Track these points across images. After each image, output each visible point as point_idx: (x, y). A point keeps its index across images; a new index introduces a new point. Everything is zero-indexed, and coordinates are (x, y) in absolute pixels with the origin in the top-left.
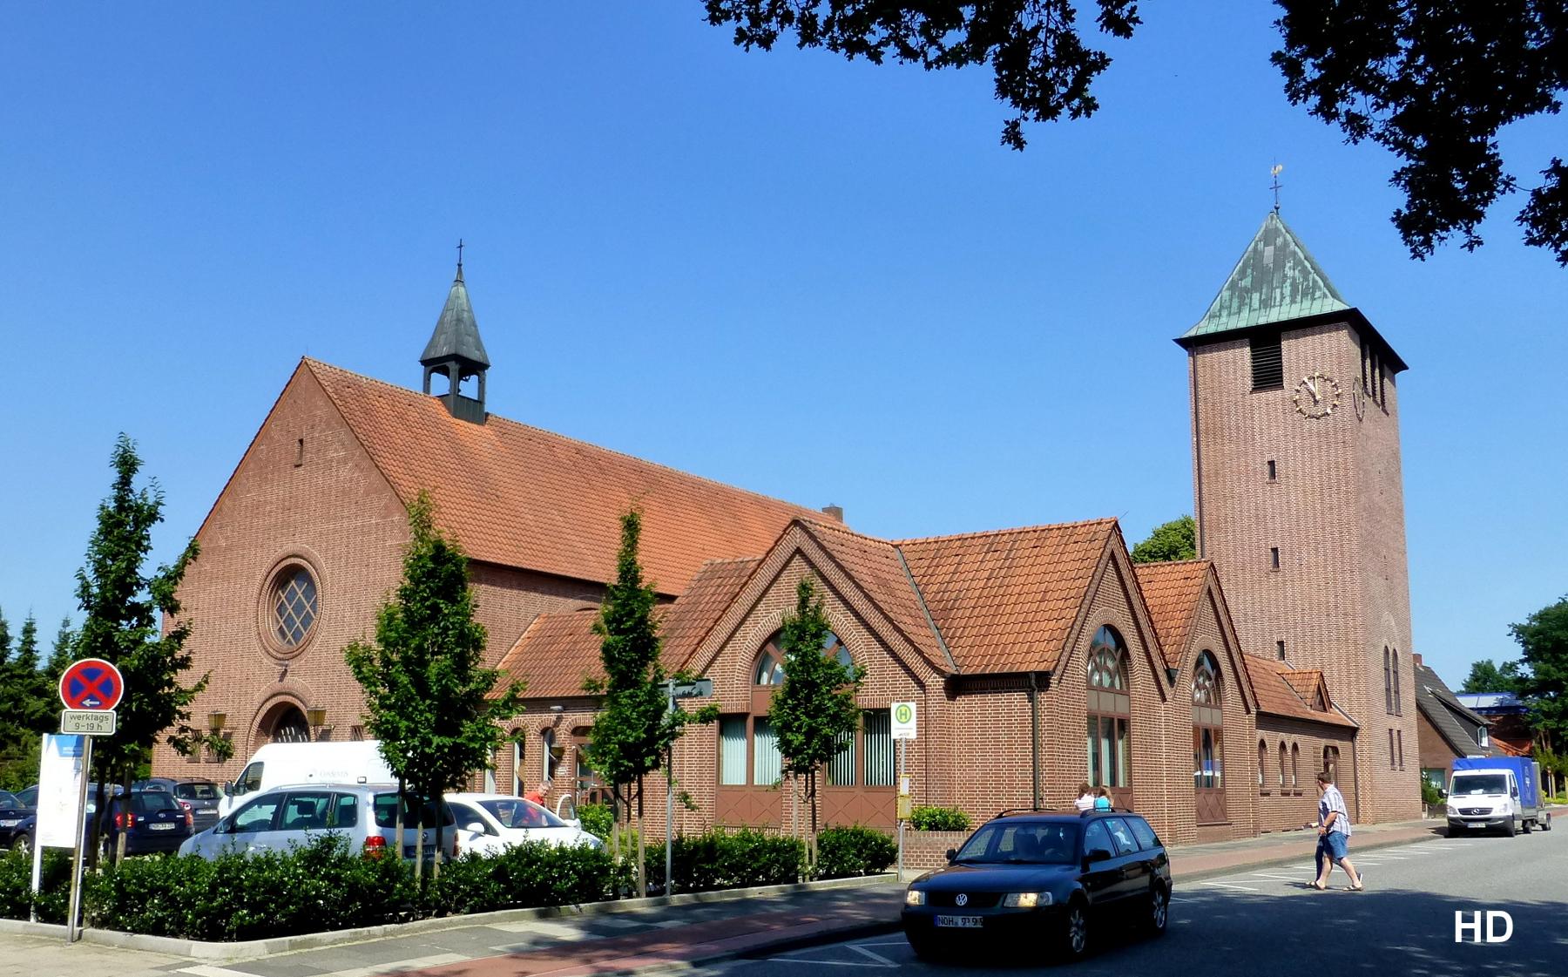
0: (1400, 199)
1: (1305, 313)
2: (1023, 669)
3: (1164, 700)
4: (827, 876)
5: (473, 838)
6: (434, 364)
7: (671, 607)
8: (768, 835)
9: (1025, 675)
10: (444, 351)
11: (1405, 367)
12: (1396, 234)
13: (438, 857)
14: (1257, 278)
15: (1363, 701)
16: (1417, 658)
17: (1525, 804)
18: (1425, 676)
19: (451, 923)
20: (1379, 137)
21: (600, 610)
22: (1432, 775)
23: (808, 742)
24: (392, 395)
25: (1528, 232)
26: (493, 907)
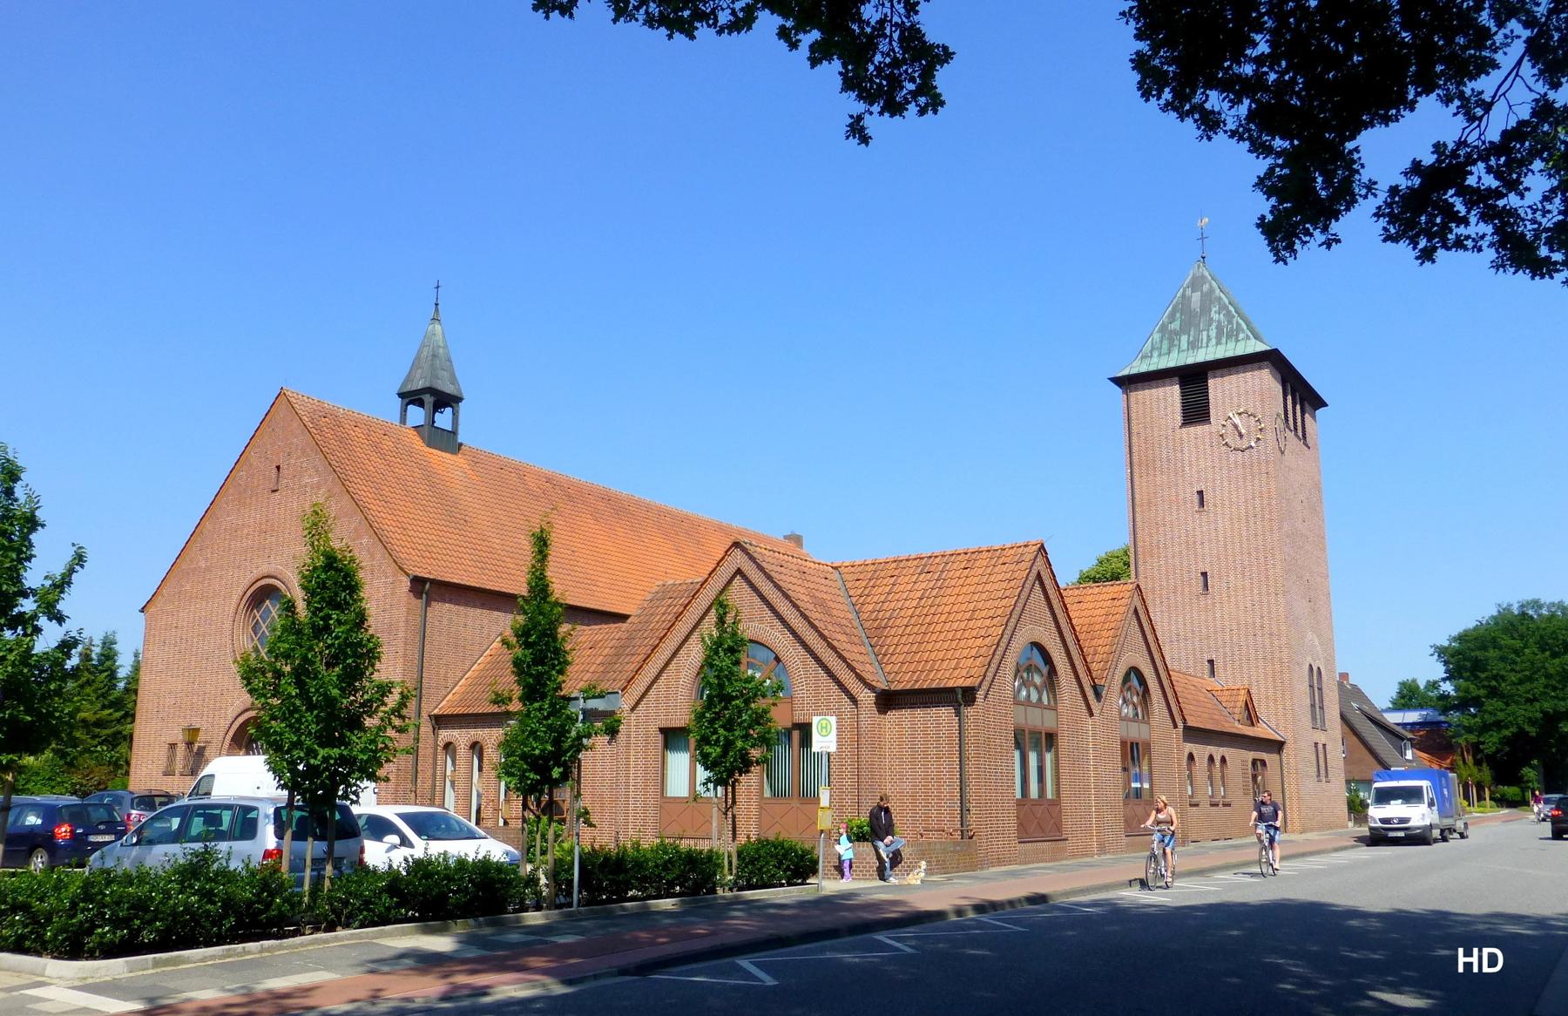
0: (1264, 206)
1: (1230, 354)
2: (950, 684)
3: (1091, 715)
4: (751, 887)
5: (388, 851)
6: (411, 397)
7: (624, 626)
8: (684, 845)
9: (952, 690)
10: (420, 384)
11: (1325, 405)
12: (1261, 241)
13: (329, 870)
14: (1188, 319)
15: (1289, 716)
16: (1344, 676)
17: (1442, 814)
18: (1350, 693)
19: (336, 939)
20: (1233, 134)
21: (505, 623)
22: (1361, 787)
23: (725, 754)
24: (368, 426)
25: (1385, 229)
26: (384, 921)
